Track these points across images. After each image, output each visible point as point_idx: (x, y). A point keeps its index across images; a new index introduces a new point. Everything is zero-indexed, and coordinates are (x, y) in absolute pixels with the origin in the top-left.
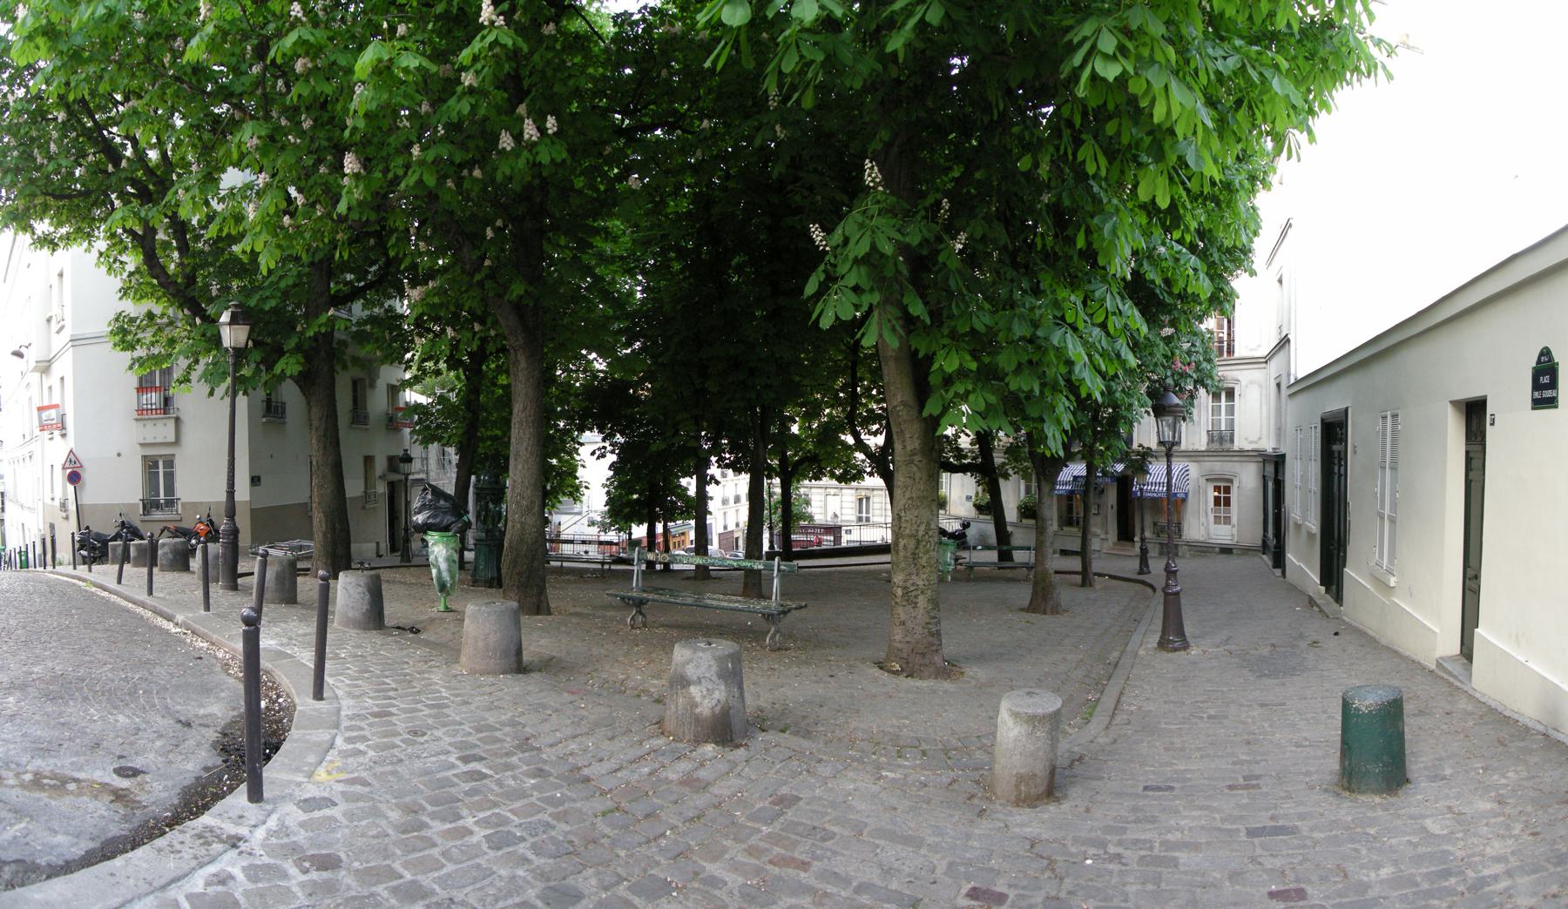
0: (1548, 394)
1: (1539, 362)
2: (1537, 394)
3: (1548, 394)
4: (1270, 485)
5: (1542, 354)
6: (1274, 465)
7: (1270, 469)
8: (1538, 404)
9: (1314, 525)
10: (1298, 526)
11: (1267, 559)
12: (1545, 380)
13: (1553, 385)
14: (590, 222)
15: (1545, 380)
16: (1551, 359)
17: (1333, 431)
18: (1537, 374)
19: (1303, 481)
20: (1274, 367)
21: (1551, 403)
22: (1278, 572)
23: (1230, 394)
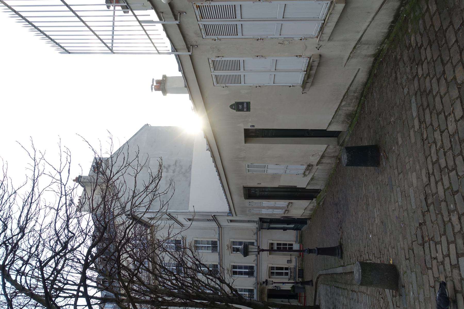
0: (245, 105)
1: (234, 109)
2: (245, 110)
3: (245, 105)
4: (272, 226)
5: (232, 108)
6: (266, 223)
7: (265, 225)
8: (248, 109)
9: (282, 203)
10: (287, 211)
11: (305, 227)
12: (240, 106)
13: (242, 103)
14: (114, 297)
15: (240, 106)
16: (233, 105)
17: (251, 193)
18: (238, 110)
19: (274, 208)
20: (223, 222)
21: (248, 104)
22: (309, 222)
23: (196, 242)
